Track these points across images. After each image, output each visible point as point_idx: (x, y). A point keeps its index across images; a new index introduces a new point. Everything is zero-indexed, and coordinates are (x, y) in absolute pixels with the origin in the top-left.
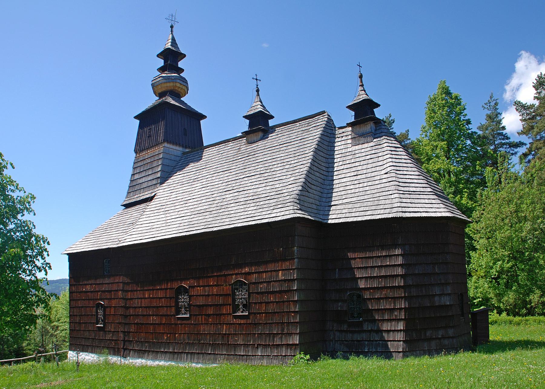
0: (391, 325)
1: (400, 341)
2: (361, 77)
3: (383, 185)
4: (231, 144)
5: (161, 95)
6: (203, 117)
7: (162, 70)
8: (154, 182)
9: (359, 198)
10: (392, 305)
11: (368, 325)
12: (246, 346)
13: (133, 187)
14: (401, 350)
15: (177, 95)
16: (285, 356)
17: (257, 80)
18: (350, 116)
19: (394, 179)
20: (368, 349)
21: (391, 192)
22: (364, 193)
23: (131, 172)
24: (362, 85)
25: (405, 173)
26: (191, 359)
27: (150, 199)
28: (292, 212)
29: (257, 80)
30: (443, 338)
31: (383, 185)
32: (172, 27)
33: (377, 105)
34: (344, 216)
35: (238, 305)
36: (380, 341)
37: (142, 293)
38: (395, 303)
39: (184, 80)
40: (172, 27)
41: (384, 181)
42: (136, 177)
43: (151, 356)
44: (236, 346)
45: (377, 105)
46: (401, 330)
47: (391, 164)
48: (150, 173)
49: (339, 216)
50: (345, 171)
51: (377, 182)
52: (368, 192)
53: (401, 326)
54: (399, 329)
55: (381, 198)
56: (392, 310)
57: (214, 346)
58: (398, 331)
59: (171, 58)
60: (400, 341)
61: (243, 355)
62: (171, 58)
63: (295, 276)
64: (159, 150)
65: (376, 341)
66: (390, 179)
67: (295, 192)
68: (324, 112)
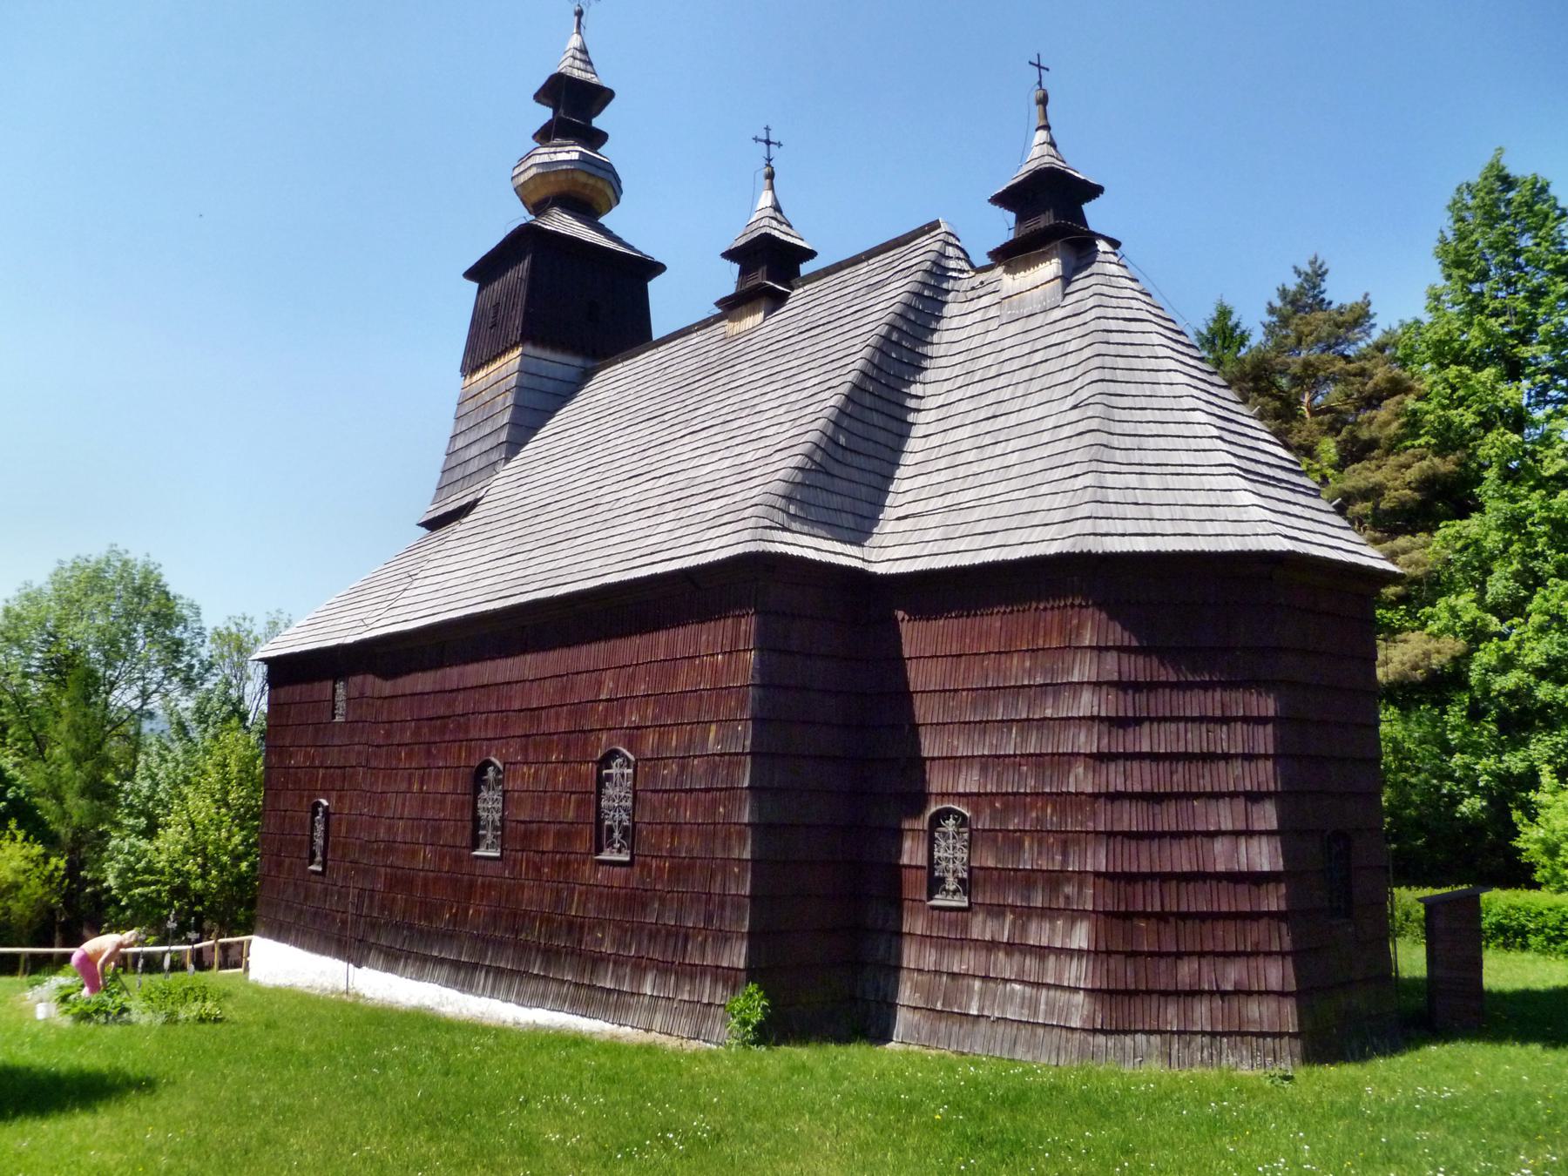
0: (1053, 930)
1: (1076, 989)
2: (1043, 101)
3: (1060, 447)
4: (695, 338)
5: (539, 208)
6: (656, 268)
7: (545, 135)
8: (494, 457)
9: (987, 491)
10: (1058, 858)
11: (984, 922)
12: (619, 962)
13: (454, 471)
14: (1076, 1023)
15: (588, 211)
16: (710, 1004)
17: (768, 142)
18: (1003, 226)
19: (1094, 424)
20: (981, 1008)
21: (1075, 470)
22: (1002, 474)
23: (449, 428)
24: (1047, 127)
25: (1143, 402)
26: (493, 988)
27: (472, 506)
28: (746, 535)
29: (768, 142)
30: (1242, 993)
31: (1060, 447)
32: (579, 14)
33: (1094, 191)
34: (929, 549)
35: (611, 830)
36: (1015, 981)
37: (403, 781)
38: (1065, 854)
39: (608, 169)
40: (579, 14)
41: (1067, 431)
42: (460, 443)
43: (410, 970)
44: (596, 962)
45: (1094, 191)
46: (1080, 952)
47: (1096, 375)
48: (488, 430)
49: (914, 550)
50: (963, 406)
51: (1046, 437)
52: (1014, 472)
53: (1080, 937)
54: (1075, 946)
55: (1044, 489)
56: (1054, 880)
57: (551, 955)
58: (1070, 953)
59: (574, 104)
60: (1076, 989)
61: (609, 991)
62: (574, 104)
63: (748, 743)
64: (513, 359)
65: (1006, 981)
66: (1081, 427)
67: (779, 475)
68: (935, 225)
